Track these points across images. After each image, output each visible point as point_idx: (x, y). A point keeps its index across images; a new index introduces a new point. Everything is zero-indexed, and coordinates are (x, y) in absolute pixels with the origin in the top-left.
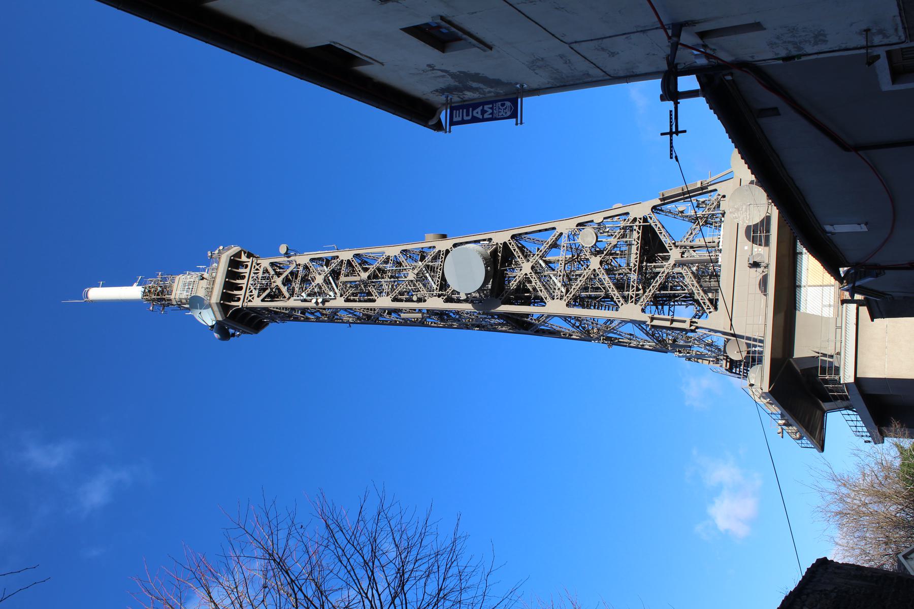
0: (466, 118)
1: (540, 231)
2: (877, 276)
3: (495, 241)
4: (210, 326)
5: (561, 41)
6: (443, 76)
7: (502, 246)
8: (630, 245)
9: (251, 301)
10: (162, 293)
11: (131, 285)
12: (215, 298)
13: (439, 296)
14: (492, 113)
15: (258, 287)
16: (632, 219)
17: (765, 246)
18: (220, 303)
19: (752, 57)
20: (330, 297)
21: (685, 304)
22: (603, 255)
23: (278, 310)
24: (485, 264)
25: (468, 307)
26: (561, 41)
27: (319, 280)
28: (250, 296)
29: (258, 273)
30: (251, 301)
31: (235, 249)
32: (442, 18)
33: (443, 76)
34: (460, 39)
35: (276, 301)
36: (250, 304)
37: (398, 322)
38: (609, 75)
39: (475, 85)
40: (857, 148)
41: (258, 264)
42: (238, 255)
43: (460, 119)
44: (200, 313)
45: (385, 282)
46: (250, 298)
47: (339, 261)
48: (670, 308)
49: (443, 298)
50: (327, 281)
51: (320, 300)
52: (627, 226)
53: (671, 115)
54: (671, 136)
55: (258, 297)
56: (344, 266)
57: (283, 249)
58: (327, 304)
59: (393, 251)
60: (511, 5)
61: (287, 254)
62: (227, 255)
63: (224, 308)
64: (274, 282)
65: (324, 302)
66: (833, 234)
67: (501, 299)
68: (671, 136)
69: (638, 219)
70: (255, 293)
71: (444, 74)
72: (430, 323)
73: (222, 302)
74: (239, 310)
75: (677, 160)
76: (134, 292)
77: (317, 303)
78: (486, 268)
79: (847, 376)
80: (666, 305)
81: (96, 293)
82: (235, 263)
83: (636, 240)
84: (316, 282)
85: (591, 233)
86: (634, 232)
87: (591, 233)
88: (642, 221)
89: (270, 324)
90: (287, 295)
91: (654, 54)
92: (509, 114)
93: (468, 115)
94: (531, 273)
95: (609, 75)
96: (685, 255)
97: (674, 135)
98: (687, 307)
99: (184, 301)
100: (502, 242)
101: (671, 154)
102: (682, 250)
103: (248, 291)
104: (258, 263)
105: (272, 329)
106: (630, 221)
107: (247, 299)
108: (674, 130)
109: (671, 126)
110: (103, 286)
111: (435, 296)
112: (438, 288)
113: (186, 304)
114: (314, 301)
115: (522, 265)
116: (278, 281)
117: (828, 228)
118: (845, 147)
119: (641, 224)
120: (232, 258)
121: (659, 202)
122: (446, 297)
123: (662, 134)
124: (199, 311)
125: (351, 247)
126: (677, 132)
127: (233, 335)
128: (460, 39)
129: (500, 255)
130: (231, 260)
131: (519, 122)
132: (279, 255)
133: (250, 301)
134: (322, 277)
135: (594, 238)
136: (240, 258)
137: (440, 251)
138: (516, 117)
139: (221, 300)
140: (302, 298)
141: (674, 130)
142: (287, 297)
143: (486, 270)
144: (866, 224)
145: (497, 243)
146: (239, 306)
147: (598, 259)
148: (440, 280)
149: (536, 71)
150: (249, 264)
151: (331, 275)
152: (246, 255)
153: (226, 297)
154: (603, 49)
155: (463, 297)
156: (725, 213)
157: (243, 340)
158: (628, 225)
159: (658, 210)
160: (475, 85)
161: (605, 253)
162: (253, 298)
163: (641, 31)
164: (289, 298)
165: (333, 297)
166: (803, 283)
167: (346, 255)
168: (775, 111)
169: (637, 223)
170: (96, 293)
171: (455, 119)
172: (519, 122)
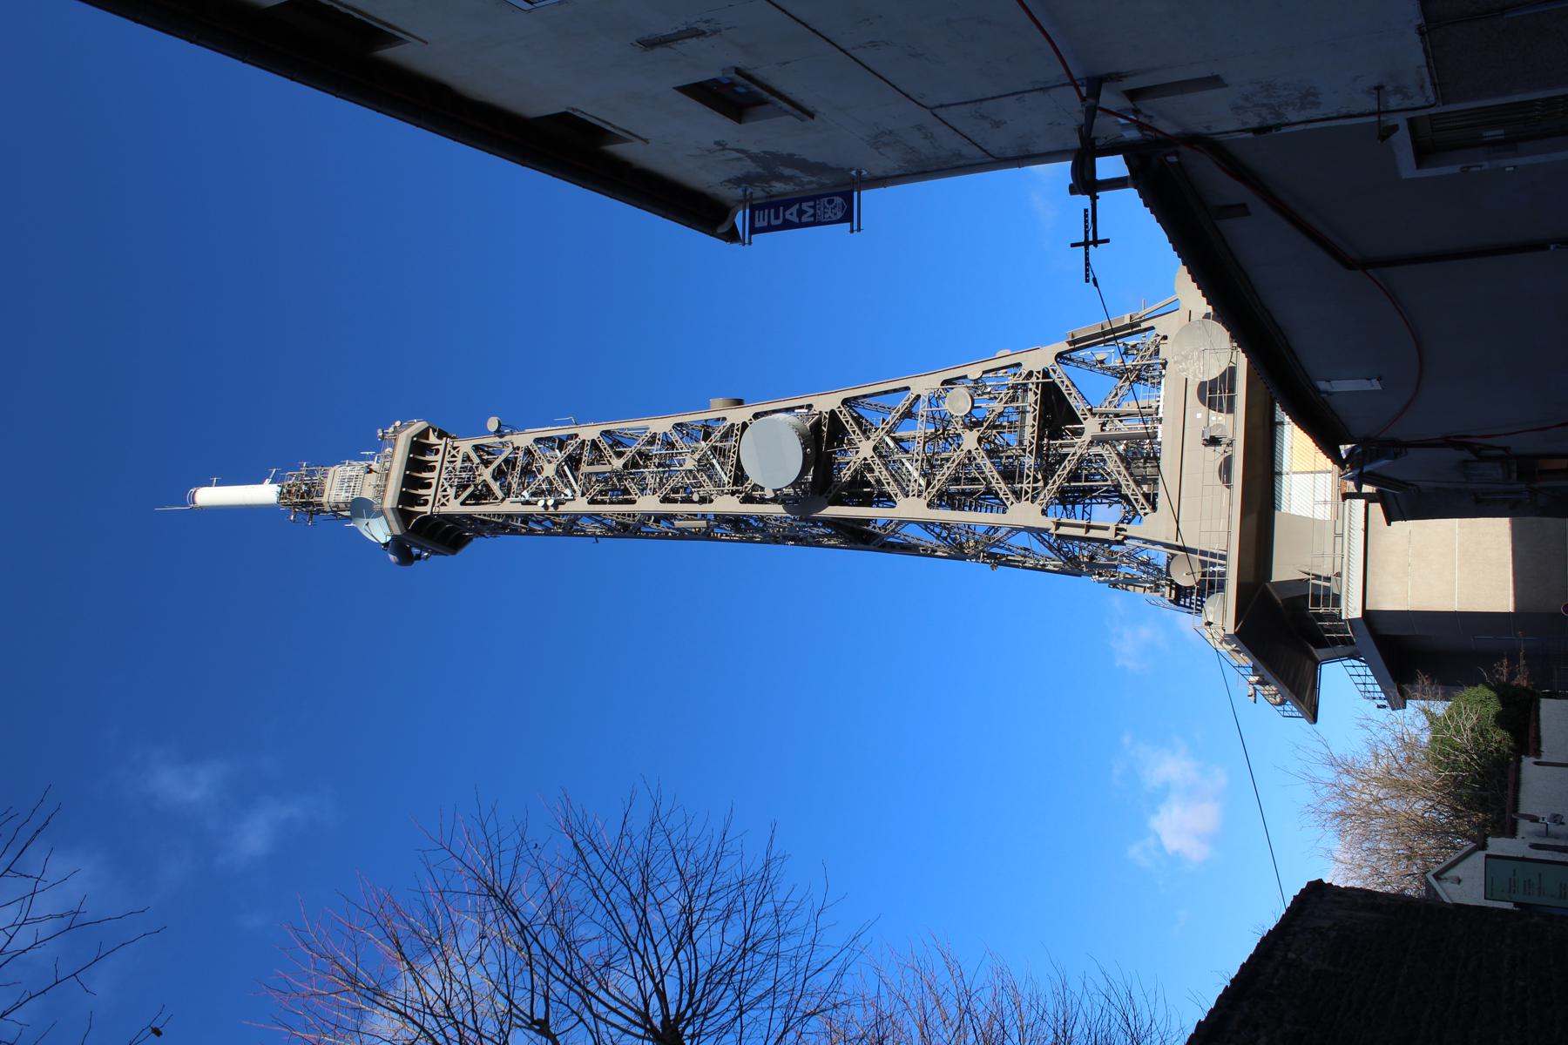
0: (774, 222)
1: (886, 392)
2: (1396, 456)
3: (817, 409)
4: (383, 544)
5: (919, 104)
6: (739, 159)
7: (827, 416)
8: (1024, 412)
9: (446, 505)
10: (308, 495)
11: (261, 482)
12: (390, 500)
13: (733, 493)
14: (814, 215)
15: (456, 484)
16: (1026, 372)
17: (1228, 412)
18: (397, 508)
19: (1208, 128)
20: (566, 498)
21: (1108, 501)
22: (982, 429)
23: (486, 518)
24: (802, 445)
25: (777, 510)
26: (919, 104)
27: (549, 470)
28: (444, 496)
29: (455, 461)
30: (446, 505)
31: (419, 426)
32: (738, 71)
33: (739, 159)
34: (763, 102)
35: (483, 504)
36: (443, 510)
37: (670, 534)
38: (992, 156)
39: (788, 172)
40: (1365, 265)
41: (454, 448)
42: (424, 434)
43: (765, 224)
44: (367, 524)
45: (650, 473)
46: (443, 500)
47: (579, 441)
48: (1084, 508)
49: (738, 497)
50: (560, 473)
51: (551, 502)
52: (1019, 384)
53: (1086, 216)
54: (1087, 248)
55: (456, 498)
56: (587, 448)
57: (492, 424)
58: (562, 508)
59: (661, 425)
60: (842, 50)
61: (499, 433)
62: (408, 436)
63: (403, 515)
64: (480, 475)
65: (556, 505)
66: (1330, 394)
67: (827, 497)
68: (1087, 248)
69: (1035, 373)
70: (451, 492)
71: (742, 155)
72: (719, 535)
73: (400, 506)
74: (427, 519)
75: (1096, 284)
76: (265, 493)
77: (546, 506)
78: (804, 449)
79: (1352, 609)
80: (1079, 503)
81: (209, 496)
82: (419, 447)
83: (1033, 405)
84: (545, 474)
85: (965, 396)
86: (1029, 393)
87: (965, 396)
88: (1040, 376)
89: (475, 539)
90: (500, 494)
91: (1059, 124)
92: (840, 215)
93: (777, 217)
94: (872, 457)
95: (992, 156)
96: (1107, 428)
97: (1091, 247)
98: (1110, 506)
99: (342, 506)
100: (828, 410)
101: (1087, 276)
102: (1102, 420)
103: (440, 490)
104: (455, 445)
105: (478, 547)
106: (1023, 376)
107: (439, 502)
108: (1091, 239)
109: (1086, 233)
110: (218, 485)
111: (727, 493)
112: (731, 481)
113: (344, 511)
114: (541, 503)
115: (859, 445)
116: (486, 474)
117: (1323, 385)
118: (1348, 263)
119: (1040, 380)
120: (415, 439)
121: (1067, 347)
122: (743, 495)
123: (1073, 245)
124: (366, 521)
125: (597, 420)
126: (1096, 242)
127: (419, 557)
128: (763, 102)
129: (825, 430)
130: (412, 442)
131: (855, 228)
132: (487, 433)
133: (443, 504)
134: (553, 466)
135: (968, 404)
136: (428, 439)
137: (733, 425)
138: (851, 220)
139: (399, 504)
140: (523, 499)
141: (1091, 239)
142: (500, 498)
143: (805, 454)
144: (1379, 379)
145: (820, 412)
146: (426, 513)
147: (975, 434)
148: (733, 470)
149: (881, 150)
150: (441, 448)
151: (566, 464)
152: (436, 434)
153: (408, 498)
154: (983, 117)
155: (769, 494)
156: (1166, 363)
157: (433, 565)
158: (1020, 382)
159: (1066, 358)
160: (788, 172)
161: (985, 425)
162: (448, 500)
163: (1041, 89)
164: (503, 499)
165: (570, 497)
166: (1285, 469)
167: (590, 432)
168: (1242, 210)
169: (1034, 379)
170: (209, 496)
171: (758, 225)
172: (855, 228)
